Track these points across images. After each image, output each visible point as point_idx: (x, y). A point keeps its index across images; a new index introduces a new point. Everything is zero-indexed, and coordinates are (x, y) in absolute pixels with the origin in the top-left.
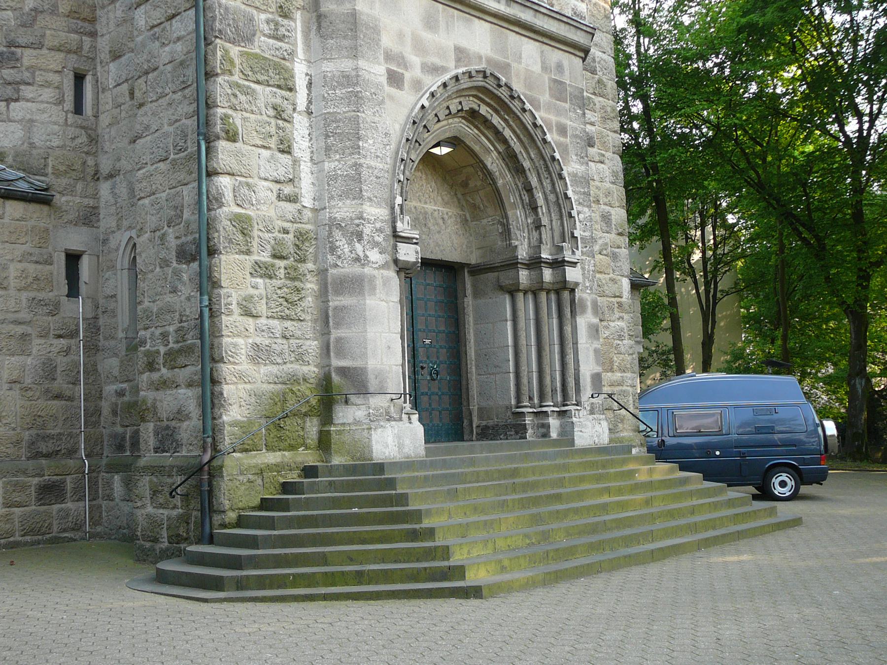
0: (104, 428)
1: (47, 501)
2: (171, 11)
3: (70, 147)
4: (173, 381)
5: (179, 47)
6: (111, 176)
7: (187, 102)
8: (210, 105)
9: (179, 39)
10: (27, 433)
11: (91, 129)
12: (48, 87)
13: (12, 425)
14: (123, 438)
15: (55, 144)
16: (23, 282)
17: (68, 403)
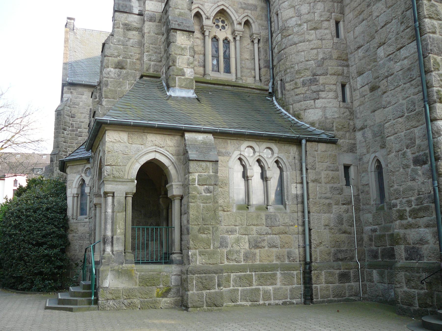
0: (365, 247)
2: (399, 46)
4: (416, 225)
5: (406, 62)
6: (362, 129)
7: (413, 87)
8: (429, 86)
9: (405, 58)
10: (333, 249)
11: (350, 108)
14: (377, 252)
15: (336, 117)
17: (349, 235)
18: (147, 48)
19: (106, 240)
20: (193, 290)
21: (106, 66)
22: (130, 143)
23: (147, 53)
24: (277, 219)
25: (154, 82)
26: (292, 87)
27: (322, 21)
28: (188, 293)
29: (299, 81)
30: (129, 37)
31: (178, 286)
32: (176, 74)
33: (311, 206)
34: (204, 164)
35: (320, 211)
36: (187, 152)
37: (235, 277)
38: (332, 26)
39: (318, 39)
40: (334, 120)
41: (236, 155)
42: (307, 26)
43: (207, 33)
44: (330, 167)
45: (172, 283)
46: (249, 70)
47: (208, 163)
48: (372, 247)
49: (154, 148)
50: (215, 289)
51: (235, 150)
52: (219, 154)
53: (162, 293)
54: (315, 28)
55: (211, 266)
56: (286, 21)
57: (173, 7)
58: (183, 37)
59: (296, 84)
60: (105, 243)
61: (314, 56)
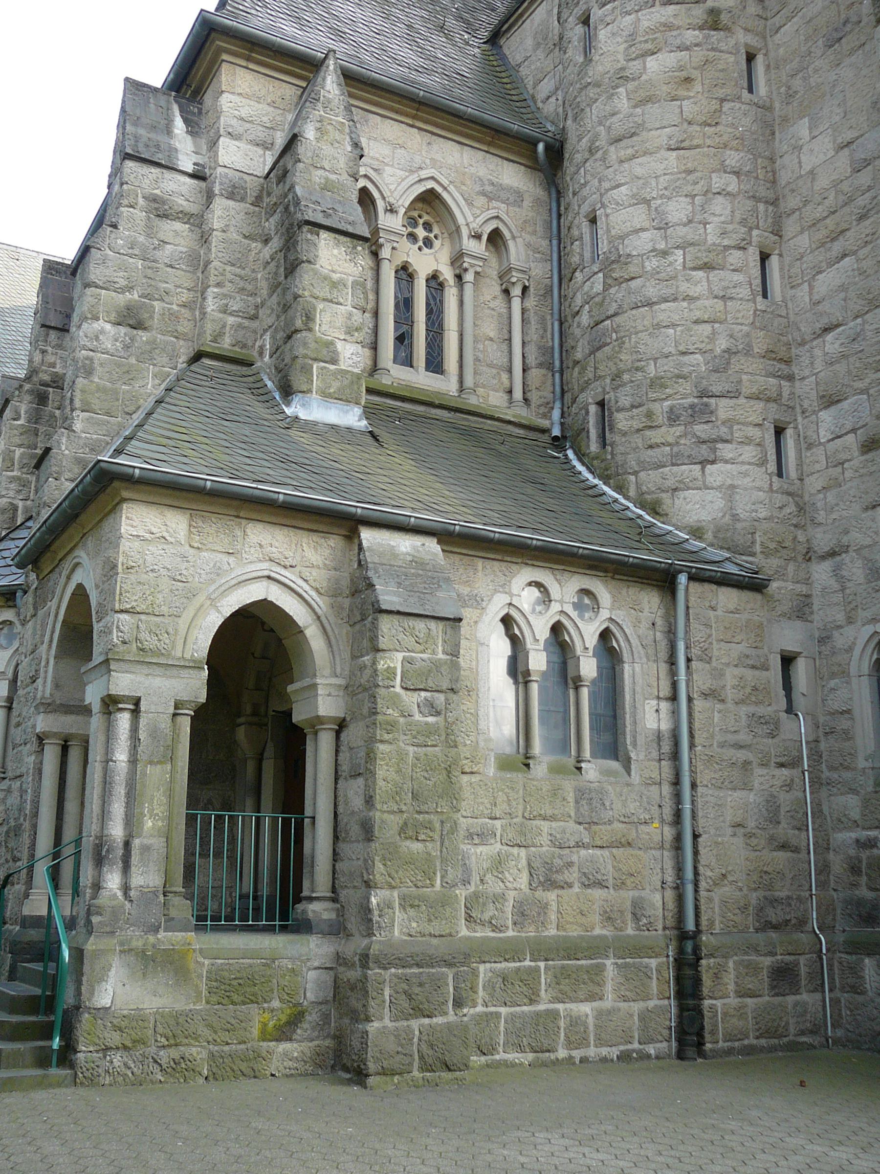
0: (835, 890)
1: (782, 990)
3: (778, 518)
6: (832, 554)
10: (754, 895)
11: (798, 496)
12: (749, 444)
13: (739, 884)
15: (761, 516)
16: (741, 693)
17: (794, 855)
18: (216, 273)
19: (108, 851)
20: (381, 1019)
21: (89, 316)
22: (196, 545)
23: (216, 290)
24: (607, 804)
25: (235, 375)
26: (636, 424)
27: (724, 246)
28: (368, 1029)
29: (660, 409)
30: (161, 236)
31: (325, 1002)
32: (313, 356)
33: (700, 767)
34: (420, 625)
35: (723, 783)
36: (371, 586)
37: (490, 974)
38: (752, 264)
39: (716, 297)
40: (755, 523)
41: (497, 607)
42: (684, 258)
43: (385, 253)
44: (748, 656)
45: (308, 995)
46: (494, 371)
47: (432, 624)
48: (857, 892)
49: (264, 568)
50: (446, 1014)
51: (496, 591)
52: (462, 601)
53: (277, 1028)
54: (706, 264)
55: (435, 941)
56: (622, 238)
57: (310, 161)
58: (335, 252)
59: (649, 415)
60: (100, 861)
61: (702, 342)
